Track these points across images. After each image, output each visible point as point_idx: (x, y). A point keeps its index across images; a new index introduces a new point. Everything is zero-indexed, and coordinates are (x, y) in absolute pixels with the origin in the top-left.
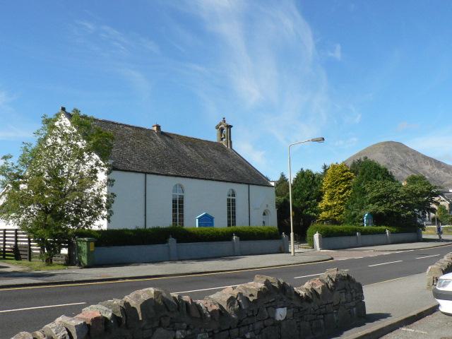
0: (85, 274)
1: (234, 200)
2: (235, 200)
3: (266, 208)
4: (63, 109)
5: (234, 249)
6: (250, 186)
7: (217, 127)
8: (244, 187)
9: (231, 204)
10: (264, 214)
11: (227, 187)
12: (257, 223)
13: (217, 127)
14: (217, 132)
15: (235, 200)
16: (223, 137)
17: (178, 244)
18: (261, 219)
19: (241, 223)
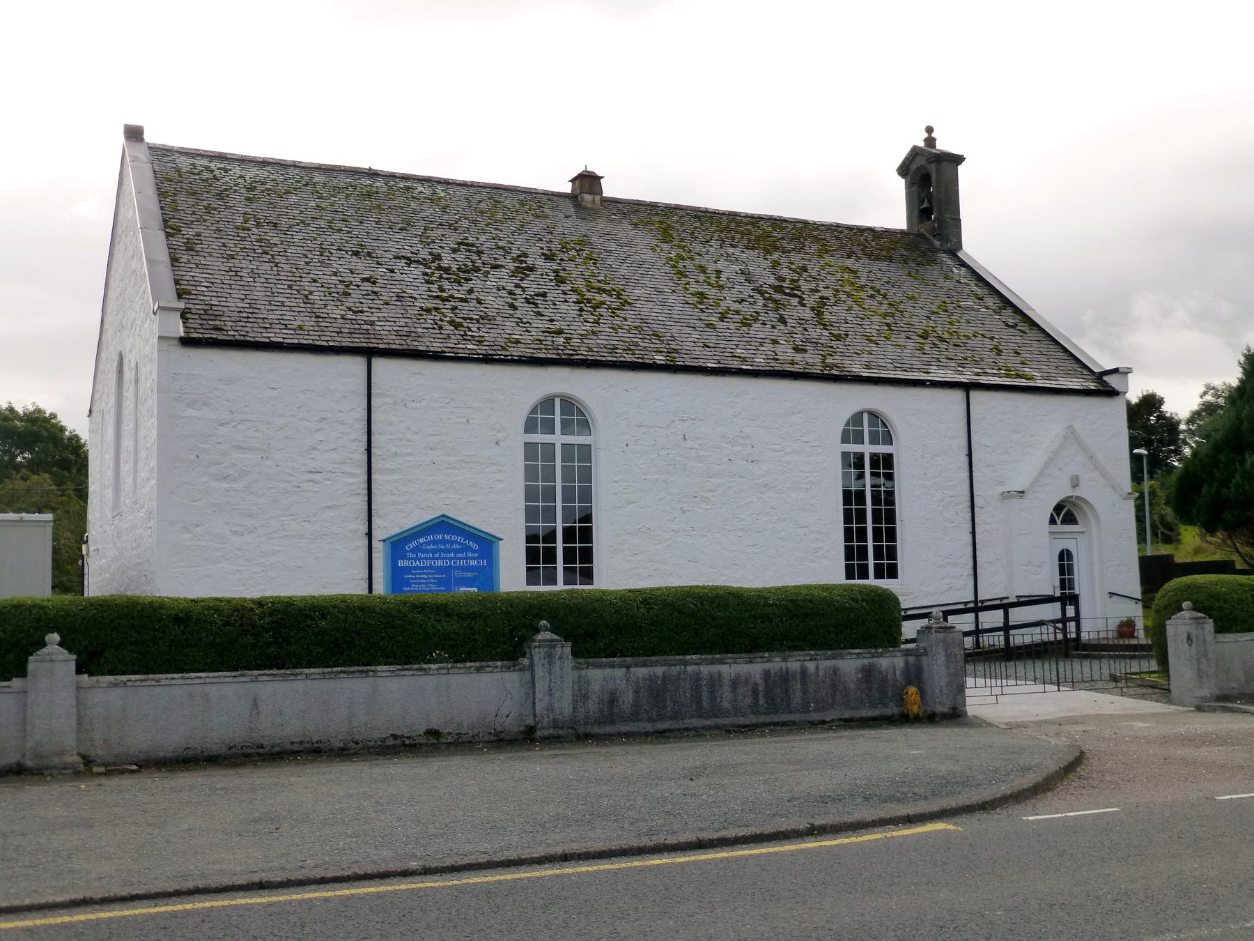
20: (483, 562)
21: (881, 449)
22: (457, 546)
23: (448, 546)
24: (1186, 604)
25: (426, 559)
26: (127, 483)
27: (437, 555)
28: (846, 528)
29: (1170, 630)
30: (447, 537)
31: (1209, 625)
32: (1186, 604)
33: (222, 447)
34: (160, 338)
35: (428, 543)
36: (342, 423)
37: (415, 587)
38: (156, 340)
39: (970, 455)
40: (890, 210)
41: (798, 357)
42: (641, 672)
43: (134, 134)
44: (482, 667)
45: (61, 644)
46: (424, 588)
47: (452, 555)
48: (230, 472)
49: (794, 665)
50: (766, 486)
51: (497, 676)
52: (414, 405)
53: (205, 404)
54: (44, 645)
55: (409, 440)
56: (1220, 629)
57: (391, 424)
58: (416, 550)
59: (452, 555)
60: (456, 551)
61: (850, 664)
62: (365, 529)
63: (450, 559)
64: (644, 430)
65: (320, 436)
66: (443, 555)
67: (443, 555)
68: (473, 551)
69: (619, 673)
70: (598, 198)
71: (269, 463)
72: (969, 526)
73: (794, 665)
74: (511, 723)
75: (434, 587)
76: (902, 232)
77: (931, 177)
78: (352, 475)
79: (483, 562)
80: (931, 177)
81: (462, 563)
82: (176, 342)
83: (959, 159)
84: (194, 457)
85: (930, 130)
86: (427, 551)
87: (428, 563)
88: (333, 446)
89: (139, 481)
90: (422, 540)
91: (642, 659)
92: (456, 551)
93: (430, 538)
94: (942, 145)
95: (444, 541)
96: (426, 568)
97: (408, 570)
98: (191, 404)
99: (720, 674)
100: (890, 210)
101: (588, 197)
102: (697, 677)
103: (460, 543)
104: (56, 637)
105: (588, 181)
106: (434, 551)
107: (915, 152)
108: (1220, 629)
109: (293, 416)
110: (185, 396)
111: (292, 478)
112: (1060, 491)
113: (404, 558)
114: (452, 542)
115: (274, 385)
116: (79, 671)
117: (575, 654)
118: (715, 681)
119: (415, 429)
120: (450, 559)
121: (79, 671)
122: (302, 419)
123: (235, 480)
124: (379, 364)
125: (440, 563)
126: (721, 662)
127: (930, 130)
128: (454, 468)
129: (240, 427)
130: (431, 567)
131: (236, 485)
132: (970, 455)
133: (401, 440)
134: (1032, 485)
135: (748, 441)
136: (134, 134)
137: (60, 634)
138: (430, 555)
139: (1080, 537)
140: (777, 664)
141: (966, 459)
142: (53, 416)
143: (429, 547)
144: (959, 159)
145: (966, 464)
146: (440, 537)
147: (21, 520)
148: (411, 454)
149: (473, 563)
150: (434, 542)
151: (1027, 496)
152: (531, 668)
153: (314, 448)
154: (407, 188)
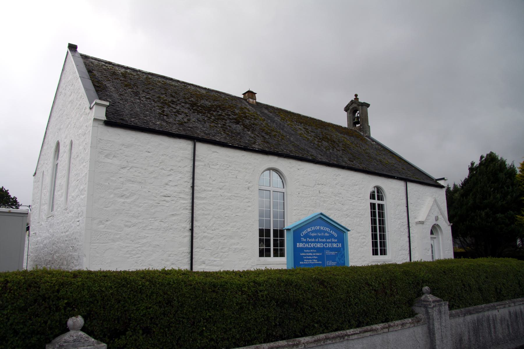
1: (381, 207)
10: (432, 233)
20: (340, 245)
21: (380, 202)
22: (327, 234)
23: (322, 234)
25: (311, 242)
26: (60, 198)
27: (317, 240)
30: (322, 228)
33: (122, 180)
34: (95, 120)
35: (312, 232)
36: (180, 173)
37: (306, 262)
38: (91, 121)
39: (407, 207)
40: (342, 120)
41: (350, 163)
42: (469, 318)
43: (73, 48)
44: (403, 325)
45: (83, 329)
47: (324, 240)
48: (125, 193)
50: (347, 215)
51: (411, 330)
52: (213, 167)
53: (114, 157)
54: (65, 330)
55: (210, 184)
57: (203, 175)
58: (306, 236)
59: (324, 240)
60: (327, 238)
62: (189, 226)
63: (324, 243)
64: (305, 187)
65: (170, 178)
66: (320, 240)
67: (320, 240)
68: (335, 238)
70: (254, 101)
71: (145, 190)
72: (407, 235)
73: (517, 308)
75: (316, 262)
76: (345, 128)
77: (357, 109)
79: (340, 245)
80: (357, 109)
81: (329, 245)
82: (102, 123)
83: (368, 105)
84: (107, 184)
85: (356, 95)
86: (311, 237)
87: (312, 245)
88: (177, 184)
89: (70, 197)
90: (309, 230)
91: (471, 308)
92: (327, 238)
93: (313, 228)
94: (361, 100)
95: (320, 231)
96: (311, 248)
97: (302, 250)
98: (107, 156)
99: (496, 315)
100: (342, 120)
101: (251, 100)
103: (328, 233)
104: (77, 321)
105: (251, 94)
106: (315, 237)
107: (352, 102)
109: (158, 167)
110: (105, 151)
111: (156, 199)
113: (300, 242)
114: (325, 232)
115: (149, 150)
117: (451, 308)
119: (214, 179)
120: (324, 243)
122: (162, 169)
123: (127, 198)
124: (199, 145)
125: (318, 245)
126: (494, 308)
127: (356, 95)
128: (230, 199)
129: (131, 170)
130: (314, 248)
131: (128, 200)
132: (407, 207)
133: (207, 183)
134: (426, 219)
135: (340, 195)
136: (73, 48)
137: (85, 318)
138: (313, 240)
139: (435, 240)
141: (406, 208)
142: (251, 94)
143: (313, 235)
144: (368, 105)
145: (406, 210)
146: (318, 228)
147: (10, 212)
148: (211, 191)
149: (335, 245)
150: (315, 231)
151: (425, 223)
152: (429, 321)
153: (167, 184)
154: (185, 86)
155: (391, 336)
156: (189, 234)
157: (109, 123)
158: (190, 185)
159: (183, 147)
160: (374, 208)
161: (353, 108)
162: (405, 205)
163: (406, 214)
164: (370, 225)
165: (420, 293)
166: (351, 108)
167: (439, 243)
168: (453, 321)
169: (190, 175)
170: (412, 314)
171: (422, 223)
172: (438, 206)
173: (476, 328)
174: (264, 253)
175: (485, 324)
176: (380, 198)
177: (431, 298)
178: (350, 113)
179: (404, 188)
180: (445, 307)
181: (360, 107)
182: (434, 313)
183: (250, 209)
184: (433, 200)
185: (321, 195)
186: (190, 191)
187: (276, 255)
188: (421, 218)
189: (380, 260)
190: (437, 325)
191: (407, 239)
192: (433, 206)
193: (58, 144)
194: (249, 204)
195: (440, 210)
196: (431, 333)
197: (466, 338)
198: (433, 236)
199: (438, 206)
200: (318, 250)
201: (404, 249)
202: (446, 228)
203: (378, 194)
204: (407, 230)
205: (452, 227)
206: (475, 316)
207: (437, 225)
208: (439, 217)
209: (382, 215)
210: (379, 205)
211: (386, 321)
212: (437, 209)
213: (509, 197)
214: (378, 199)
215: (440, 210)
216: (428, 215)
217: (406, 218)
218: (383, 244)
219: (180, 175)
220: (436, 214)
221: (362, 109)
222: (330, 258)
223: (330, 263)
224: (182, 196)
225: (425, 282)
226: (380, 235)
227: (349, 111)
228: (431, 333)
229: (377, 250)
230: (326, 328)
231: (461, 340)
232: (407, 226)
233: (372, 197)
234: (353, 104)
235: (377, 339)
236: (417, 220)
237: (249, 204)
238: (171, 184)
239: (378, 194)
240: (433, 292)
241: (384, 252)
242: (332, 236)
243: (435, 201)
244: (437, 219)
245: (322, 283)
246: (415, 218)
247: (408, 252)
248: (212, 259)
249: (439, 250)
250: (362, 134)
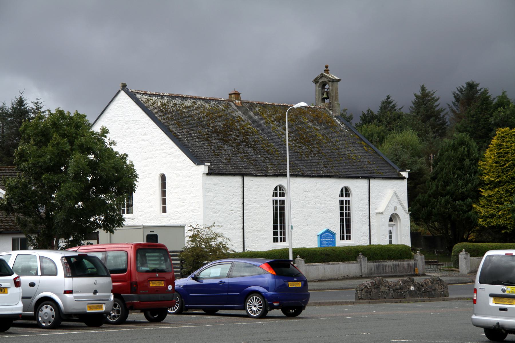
0: (313, 285)
1: (348, 202)
2: (349, 201)
3: (393, 212)
4: (124, 87)
5: (362, 272)
6: (371, 181)
7: (316, 81)
8: (362, 183)
9: (345, 209)
10: (391, 220)
11: (339, 184)
12: (380, 239)
13: (316, 81)
14: (313, 89)
15: (349, 201)
16: (325, 96)
17: (472, 258)
18: (386, 226)
19: (359, 239)
21: (347, 199)
24: (463, 250)
28: (165, 204)
29: (460, 256)
31: (469, 255)
32: (463, 250)
42: (375, 264)
46: (325, 245)
49: (397, 263)
56: (471, 256)
61: (405, 263)
62: (242, 227)
65: (233, 200)
69: (372, 264)
72: (368, 223)
73: (397, 263)
74: (358, 274)
78: (239, 211)
99: (195, 275)
101: (237, 101)
102: (383, 265)
104: (298, 256)
108: (471, 256)
112: (391, 212)
116: (305, 263)
118: (386, 266)
121: (305, 263)
131: (217, 215)
134: (385, 210)
139: (394, 227)
140: (395, 262)
141: (368, 201)
145: (368, 203)
152: (360, 263)
155: (350, 265)
156: (242, 230)
157: (209, 174)
158: (242, 202)
159: (238, 180)
160: (343, 204)
161: (323, 82)
162: (368, 199)
163: (368, 207)
164: (339, 217)
165: (359, 255)
166: (320, 81)
167: (397, 230)
168: (369, 264)
169: (241, 196)
170: (356, 260)
171: (381, 213)
172: (397, 197)
173: (378, 267)
174: (276, 240)
175: (381, 267)
176: (348, 195)
177: (361, 256)
178: (319, 87)
179: (367, 185)
180: (366, 259)
181: (331, 83)
182: (362, 260)
183: (268, 213)
184: (393, 192)
185: (307, 199)
186: (241, 206)
187: (281, 241)
188: (381, 210)
189: (280, 246)
190: (363, 263)
191: (368, 227)
192: (392, 197)
193: (163, 177)
194: (268, 210)
195: (399, 200)
196: (361, 266)
197: (373, 269)
198: (391, 223)
199: (397, 197)
200: (327, 241)
201: (365, 236)
202: (405, 218)
203: (345, 192)
204: (368, 220)
205: (410, 215)
206: (378, 263)
207: (396, 214)
208: (398, 207)
209: (348, 209)
210: (346, 201)
211: (349, 261)
212: (397, 200)
213: (470, 185)
214: (346, 196)
215: (399, 200)
216: (387, 206)
217: (368, 210)
218: (349, 232)
219: (237, 197)
220: (395, 204)
221: (332, 85)
222: (330, 244)
223: (330, 246)
224: (238, 209)
225: (360, 252)
226: (346, 224)
227: (318, 84)
228: (361, 266)
229: (343, 236)
230: (335, 261)
231: (371, 270)
232: (368, 216)
233: (341, 195)
234: (323, 78)
235: (346, 265)
236: (377, 211)
237: (268, 210)
238: (233, 203)
239: (345, 192)
240: (363, 254)
241: (349, 238)
242: (331, 236)
243: (395, 193)
244: (395, 209)
245: (333, 250)
246: (376, 209)
247: (368, 237)
248: (252, 244)
249: (397, 235)
250: (331, 113)
